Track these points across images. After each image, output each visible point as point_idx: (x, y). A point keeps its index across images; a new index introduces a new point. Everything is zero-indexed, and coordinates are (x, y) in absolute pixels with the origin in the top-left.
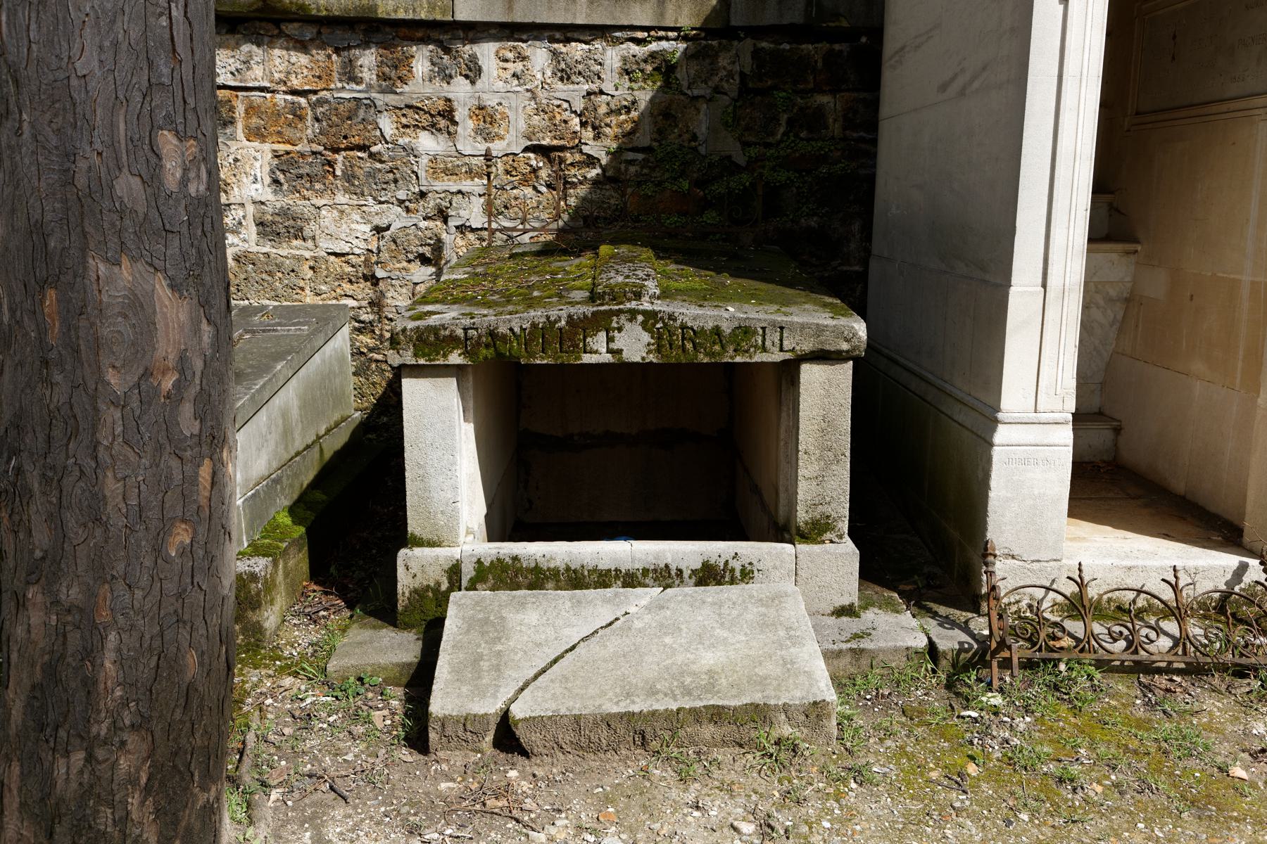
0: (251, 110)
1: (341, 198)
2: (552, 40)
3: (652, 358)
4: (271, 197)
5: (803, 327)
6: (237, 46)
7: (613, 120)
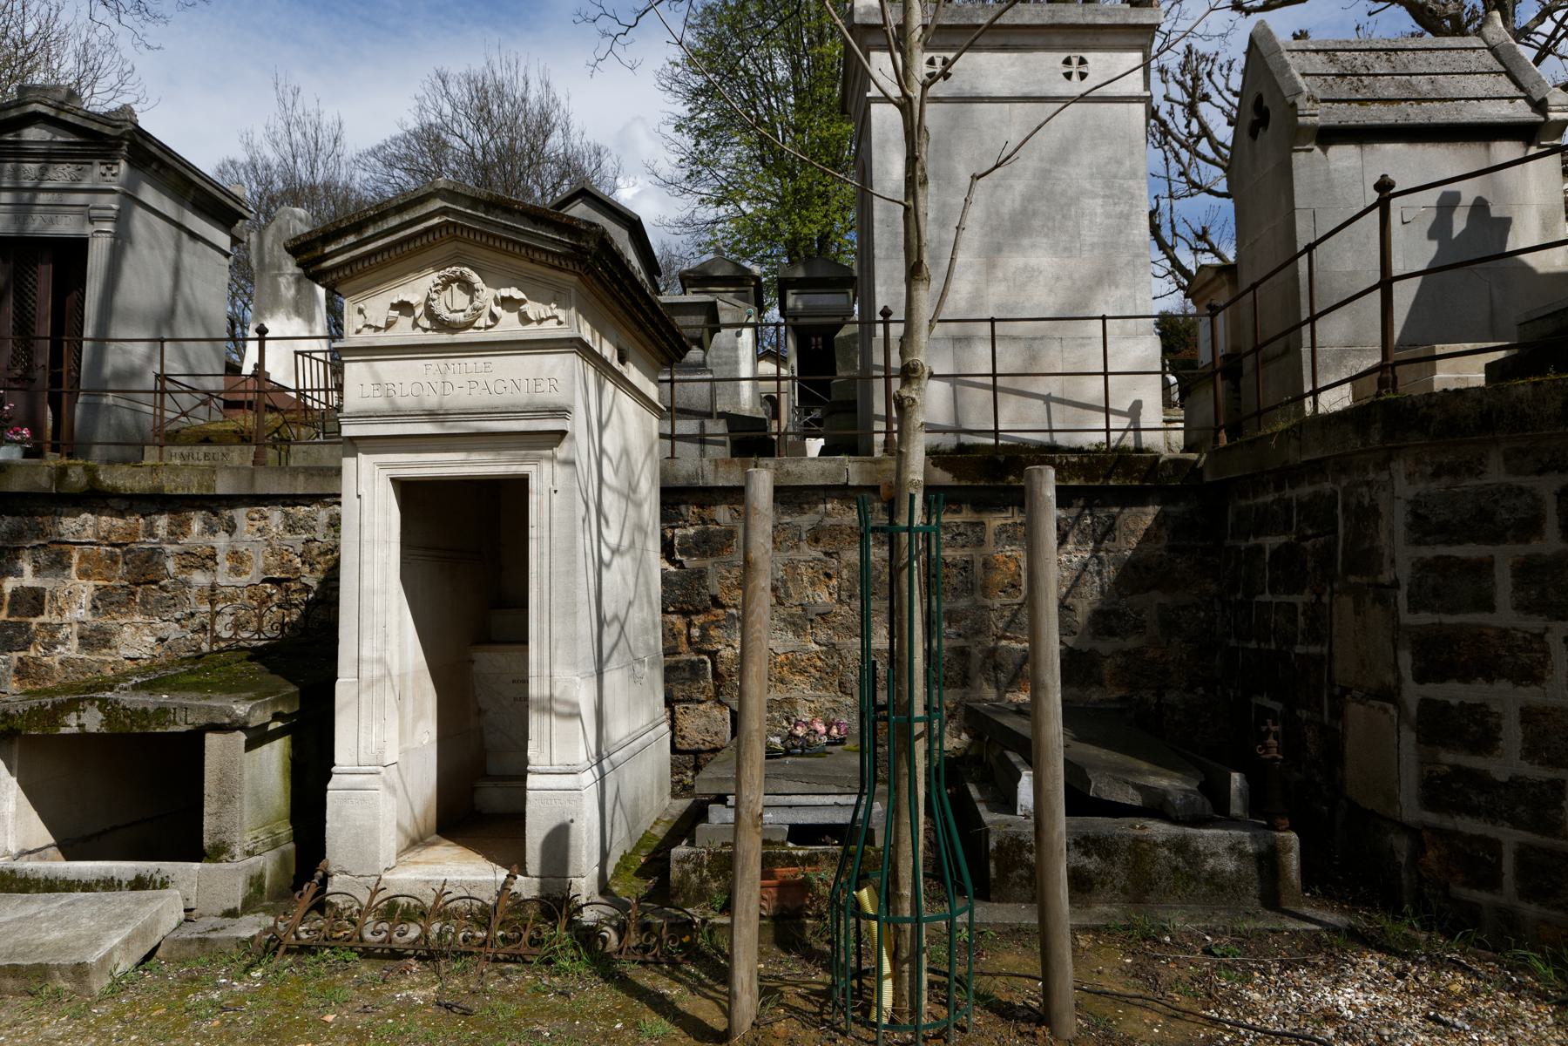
0: (83, 558)
1: (138, 618)
2: (284, 505)
3: (104, 730)
4: (90, 618)
5: (200, 707)
6: (78, 515)
7: (321, 559)
